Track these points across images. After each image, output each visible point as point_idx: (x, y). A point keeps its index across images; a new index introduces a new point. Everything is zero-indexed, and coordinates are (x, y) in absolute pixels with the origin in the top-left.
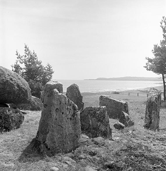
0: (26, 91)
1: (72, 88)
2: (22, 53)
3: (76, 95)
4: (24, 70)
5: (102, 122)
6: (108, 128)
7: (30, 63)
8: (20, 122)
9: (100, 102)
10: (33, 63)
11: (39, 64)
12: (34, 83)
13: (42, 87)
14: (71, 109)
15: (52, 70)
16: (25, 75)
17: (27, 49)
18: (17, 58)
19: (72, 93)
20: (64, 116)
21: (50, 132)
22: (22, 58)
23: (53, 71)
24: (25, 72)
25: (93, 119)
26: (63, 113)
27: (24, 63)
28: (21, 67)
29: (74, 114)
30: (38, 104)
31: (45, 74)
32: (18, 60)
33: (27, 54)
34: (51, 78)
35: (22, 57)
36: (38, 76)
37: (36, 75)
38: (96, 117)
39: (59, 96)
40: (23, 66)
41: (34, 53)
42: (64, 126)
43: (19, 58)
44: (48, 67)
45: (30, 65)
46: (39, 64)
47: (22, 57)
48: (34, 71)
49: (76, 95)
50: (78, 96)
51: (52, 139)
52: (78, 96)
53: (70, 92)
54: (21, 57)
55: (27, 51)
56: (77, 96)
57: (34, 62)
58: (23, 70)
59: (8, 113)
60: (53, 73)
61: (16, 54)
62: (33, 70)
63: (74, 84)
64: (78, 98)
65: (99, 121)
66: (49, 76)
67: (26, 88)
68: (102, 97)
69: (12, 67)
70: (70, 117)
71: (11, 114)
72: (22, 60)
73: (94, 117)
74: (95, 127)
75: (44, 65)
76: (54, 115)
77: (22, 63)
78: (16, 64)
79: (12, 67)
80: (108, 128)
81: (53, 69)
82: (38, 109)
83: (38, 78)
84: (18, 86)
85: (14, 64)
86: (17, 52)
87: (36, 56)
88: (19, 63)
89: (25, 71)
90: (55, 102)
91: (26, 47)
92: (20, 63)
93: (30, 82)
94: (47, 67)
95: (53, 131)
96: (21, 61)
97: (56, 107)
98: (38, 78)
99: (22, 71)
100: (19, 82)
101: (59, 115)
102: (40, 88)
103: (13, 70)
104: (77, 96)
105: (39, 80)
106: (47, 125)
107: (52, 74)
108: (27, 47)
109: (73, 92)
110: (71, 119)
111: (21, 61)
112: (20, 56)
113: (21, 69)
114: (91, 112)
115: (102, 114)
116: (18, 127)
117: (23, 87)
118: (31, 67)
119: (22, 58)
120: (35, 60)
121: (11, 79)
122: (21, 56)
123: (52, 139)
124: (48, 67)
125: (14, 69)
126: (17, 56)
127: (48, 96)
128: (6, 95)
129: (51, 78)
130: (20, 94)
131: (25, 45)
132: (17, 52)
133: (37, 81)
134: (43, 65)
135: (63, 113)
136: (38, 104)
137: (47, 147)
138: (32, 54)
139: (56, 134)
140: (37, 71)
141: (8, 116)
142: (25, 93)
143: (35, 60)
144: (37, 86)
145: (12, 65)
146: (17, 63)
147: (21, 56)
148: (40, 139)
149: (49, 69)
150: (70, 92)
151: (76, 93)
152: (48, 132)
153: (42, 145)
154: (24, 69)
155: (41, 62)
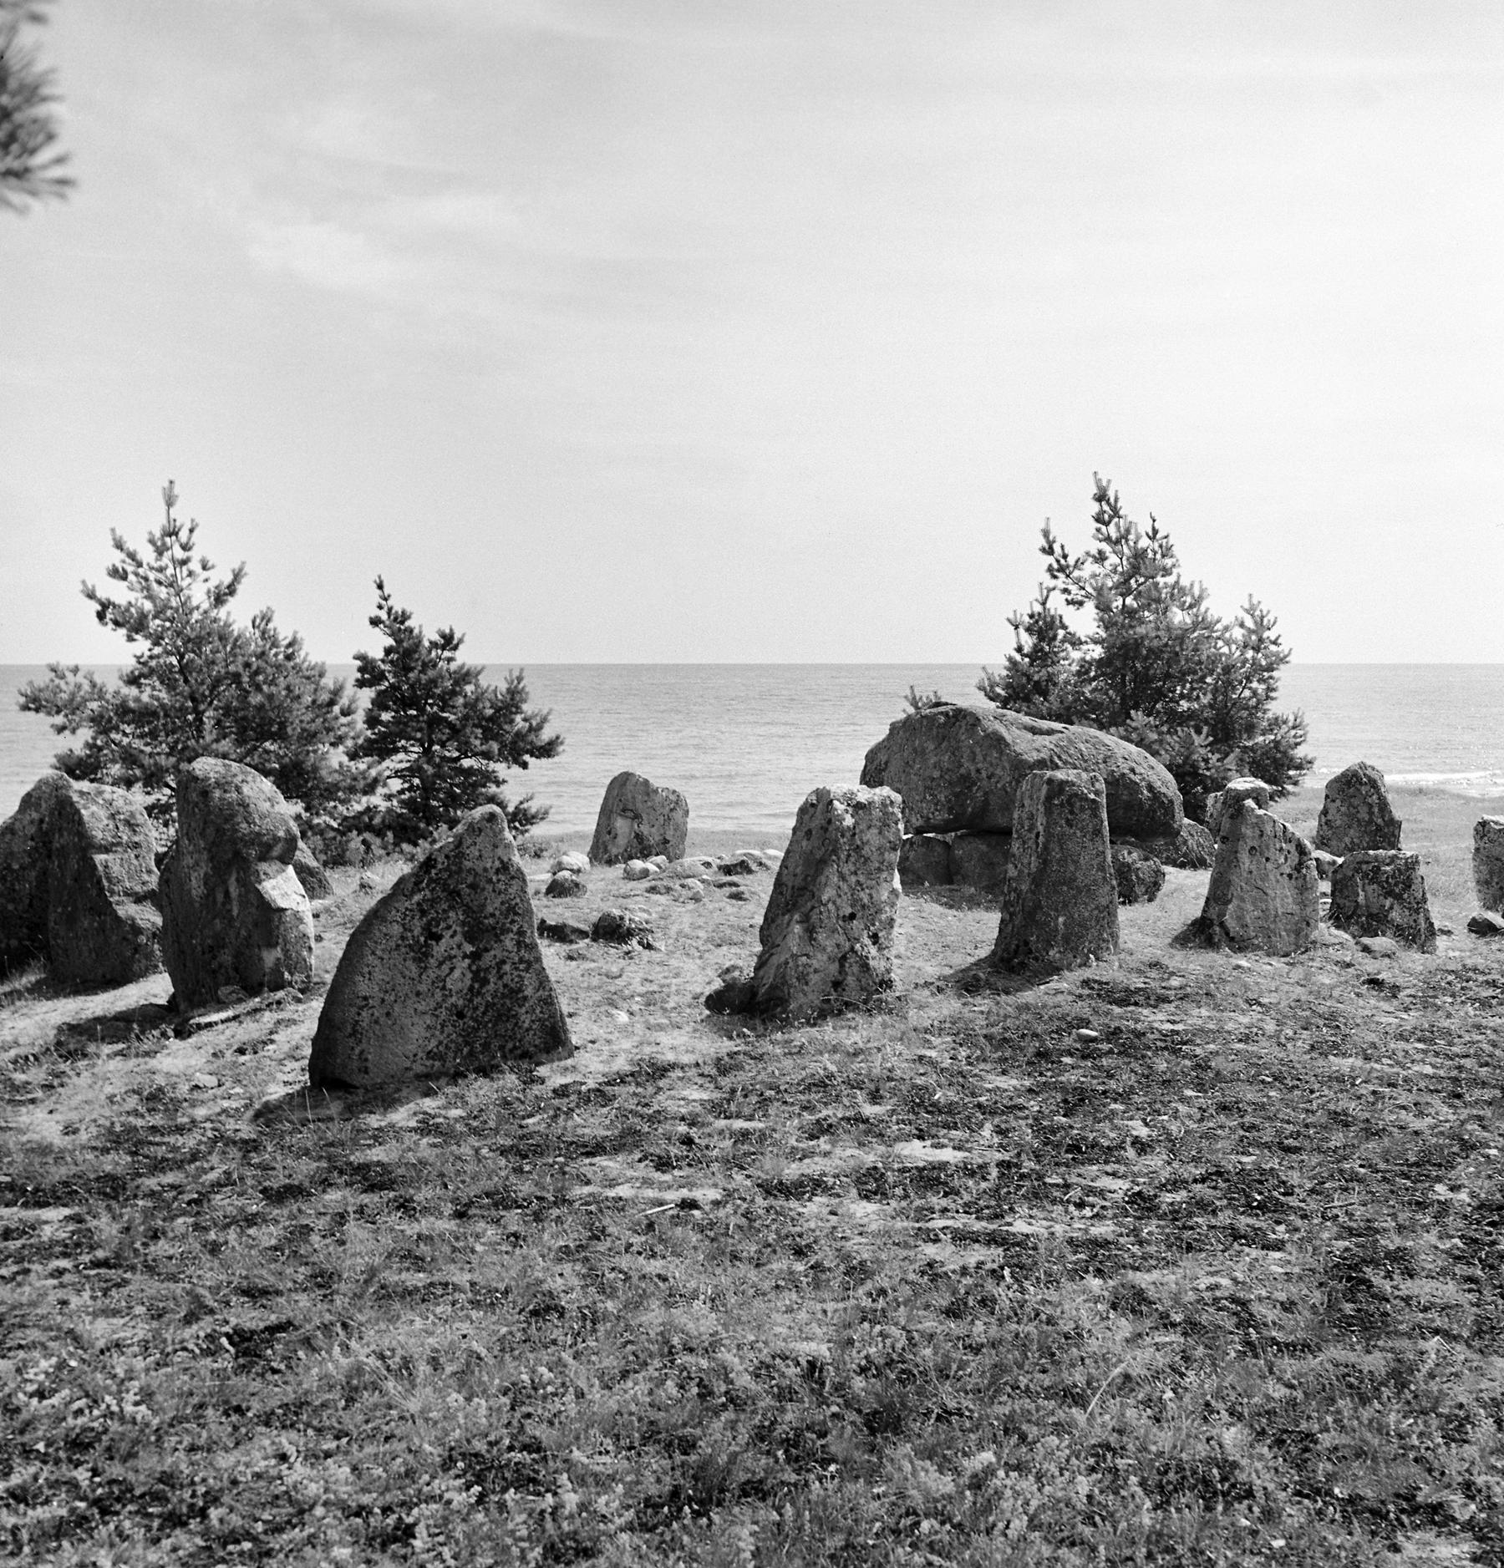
0: (1171, 802)
1: (1349, 783)
2: (1079, 537)
3: (1371, 813)
4: (1091, 646)
5: (1398, 897)
6: (1422, 921)
7: (1129, 600)
8: (1156, 886)
9: (1477, 850)
10: (1153, 600)
11: (1191, 607)
12: (1161, 734)
13: (1206, 761)
14: (1293, 850)
15: (1275, 643)
16: (1094, 679)
17: (1107, 507)
18: (1050, 569)
19: (1351, 805)
20: (1269, 866)
21: (1235, 902)
22: (1076, 573)
23: (1284, 648)
24: (1100, 663)
25: (1370, 888)
26: (1267, 859)
27: (1090, 606)
28: (1071, 630)
29: (1300, 864)
30: (1199, 845)
31: (1227, 670)
32: (1052, 583)
33: (1108, 539)
34: (1273, 694)
35: (1078, 564)
36: (1183, 682)
37: (1167, 676)
38: (1379, 884)
39: (1259, 817)
40: (1084, 622)
41: (1155, 531)
42: (1269, 892)
43: (1062, 569)
44: (1250, 623)
45: (1127, 612)
46: (1191, 607)
47: (1078, 564)
48: (1155, 653)
49: (1371, 813)
50: (1380, 821)
51: (1240, 918)
52: (1380, 821)
53: (1338, 803)
54: (1075, 566)
55: (1107, 524)
56: (1371, 821)
57: (1154, 594)
58: (1085, 647)
59: (1129, 860)
60: (1282, 660)
61: (1043, 550)
62: (1150, 650)
63: (1363, 766)
64: (1379, 829)
65: (1389, 894)
66: (1255, 685)
67: (1170, 794)
68: (1484, 824)
69: (1017, 627)
70: (1288, 871)
71: (1134, 862)
72: (1077, 582)
73: (1372, 881)
74: (1375, 911)
75: (1224, 608)
76: (1245, 860)
77: (1081, 604)
78: (1038, 608)
79: (1017, 627)
80: (1422, 921)
81: (1288, 634)
82: (1197, 863)
83: (1182, 696)
84: (1150, 788)
85: (1025, 606)
86: (1046, 534)
87: (1167, 552)
88: (1057, 603)
89: (1097, 652)
90: (1247, 831)
91: (1101, 497)
92: (1069, 602)
93: (1135, 729)
94: (1242, 625)
95: (1242, 900)
96: (1074, 588)
97: (1250, 843)
98: (1182, 696)
99: (1076, 655)
100: (1153, 778)
101: (1259, 862)
102: (1195, 767)
103: (1019, 649)
104: (1371, 821)
105: (1191, 715)
106: (1229, 884)
107: (1275, 674)
108: (1111, 494)
109: (1356, 802)
110: (1290, 876)
111: (1074, 588)
112: (1065, 557)
113: (1076, 643)
114: (1364, 867)
115: (1401, 873)
116: (1150, 900)
117: (1163, 790)
118: (1141, 630)
119: (1076, 573)
120: (1160, 580)
121: (1133, 770)
122: (1071, 561)
123: (1240, 918)
124: (1250, 623)
125: (1028, 641)
126: (1050, 560)
127: (1232, 817)
128: (1121, 812)
129: (1273, 694)
130: (1155, 811)
131: (1098, 482)
132: (1046, 534)
133: (1175, 719)
134: (1213, 614)
135: (1267, 859)
136: (1199, 845)
137: (1227, 934)
138: (1144, 543)
139: (1249, 907)
140: (1177, 654)
141: (1128, 866)
142: (1168, 808)
143: (1160, 580)
144: (1180, 754)
145: (1011, 616)
146: (1044, 604)
147: (1071, 561)
148: (1213, 914)
149: (1258, 638)
150: (1338, 803)
151: (1370, 806)
152: (1230, 901)
153: (1217, 929)
154: (1096, 642)
155: (1202, 590)
